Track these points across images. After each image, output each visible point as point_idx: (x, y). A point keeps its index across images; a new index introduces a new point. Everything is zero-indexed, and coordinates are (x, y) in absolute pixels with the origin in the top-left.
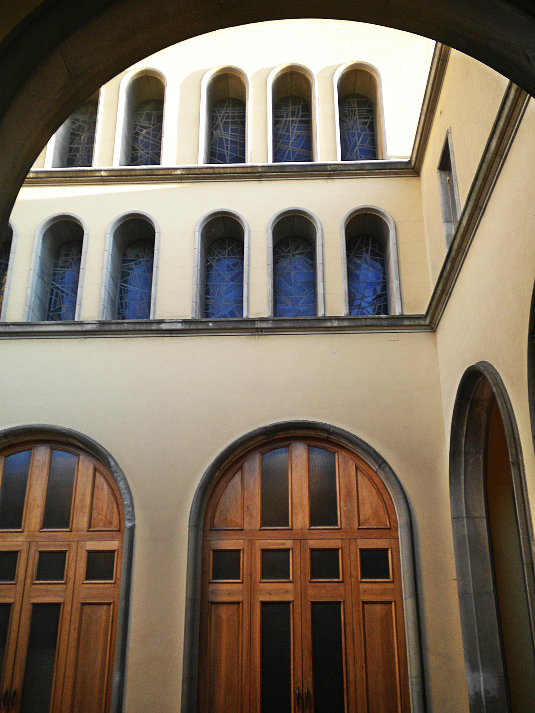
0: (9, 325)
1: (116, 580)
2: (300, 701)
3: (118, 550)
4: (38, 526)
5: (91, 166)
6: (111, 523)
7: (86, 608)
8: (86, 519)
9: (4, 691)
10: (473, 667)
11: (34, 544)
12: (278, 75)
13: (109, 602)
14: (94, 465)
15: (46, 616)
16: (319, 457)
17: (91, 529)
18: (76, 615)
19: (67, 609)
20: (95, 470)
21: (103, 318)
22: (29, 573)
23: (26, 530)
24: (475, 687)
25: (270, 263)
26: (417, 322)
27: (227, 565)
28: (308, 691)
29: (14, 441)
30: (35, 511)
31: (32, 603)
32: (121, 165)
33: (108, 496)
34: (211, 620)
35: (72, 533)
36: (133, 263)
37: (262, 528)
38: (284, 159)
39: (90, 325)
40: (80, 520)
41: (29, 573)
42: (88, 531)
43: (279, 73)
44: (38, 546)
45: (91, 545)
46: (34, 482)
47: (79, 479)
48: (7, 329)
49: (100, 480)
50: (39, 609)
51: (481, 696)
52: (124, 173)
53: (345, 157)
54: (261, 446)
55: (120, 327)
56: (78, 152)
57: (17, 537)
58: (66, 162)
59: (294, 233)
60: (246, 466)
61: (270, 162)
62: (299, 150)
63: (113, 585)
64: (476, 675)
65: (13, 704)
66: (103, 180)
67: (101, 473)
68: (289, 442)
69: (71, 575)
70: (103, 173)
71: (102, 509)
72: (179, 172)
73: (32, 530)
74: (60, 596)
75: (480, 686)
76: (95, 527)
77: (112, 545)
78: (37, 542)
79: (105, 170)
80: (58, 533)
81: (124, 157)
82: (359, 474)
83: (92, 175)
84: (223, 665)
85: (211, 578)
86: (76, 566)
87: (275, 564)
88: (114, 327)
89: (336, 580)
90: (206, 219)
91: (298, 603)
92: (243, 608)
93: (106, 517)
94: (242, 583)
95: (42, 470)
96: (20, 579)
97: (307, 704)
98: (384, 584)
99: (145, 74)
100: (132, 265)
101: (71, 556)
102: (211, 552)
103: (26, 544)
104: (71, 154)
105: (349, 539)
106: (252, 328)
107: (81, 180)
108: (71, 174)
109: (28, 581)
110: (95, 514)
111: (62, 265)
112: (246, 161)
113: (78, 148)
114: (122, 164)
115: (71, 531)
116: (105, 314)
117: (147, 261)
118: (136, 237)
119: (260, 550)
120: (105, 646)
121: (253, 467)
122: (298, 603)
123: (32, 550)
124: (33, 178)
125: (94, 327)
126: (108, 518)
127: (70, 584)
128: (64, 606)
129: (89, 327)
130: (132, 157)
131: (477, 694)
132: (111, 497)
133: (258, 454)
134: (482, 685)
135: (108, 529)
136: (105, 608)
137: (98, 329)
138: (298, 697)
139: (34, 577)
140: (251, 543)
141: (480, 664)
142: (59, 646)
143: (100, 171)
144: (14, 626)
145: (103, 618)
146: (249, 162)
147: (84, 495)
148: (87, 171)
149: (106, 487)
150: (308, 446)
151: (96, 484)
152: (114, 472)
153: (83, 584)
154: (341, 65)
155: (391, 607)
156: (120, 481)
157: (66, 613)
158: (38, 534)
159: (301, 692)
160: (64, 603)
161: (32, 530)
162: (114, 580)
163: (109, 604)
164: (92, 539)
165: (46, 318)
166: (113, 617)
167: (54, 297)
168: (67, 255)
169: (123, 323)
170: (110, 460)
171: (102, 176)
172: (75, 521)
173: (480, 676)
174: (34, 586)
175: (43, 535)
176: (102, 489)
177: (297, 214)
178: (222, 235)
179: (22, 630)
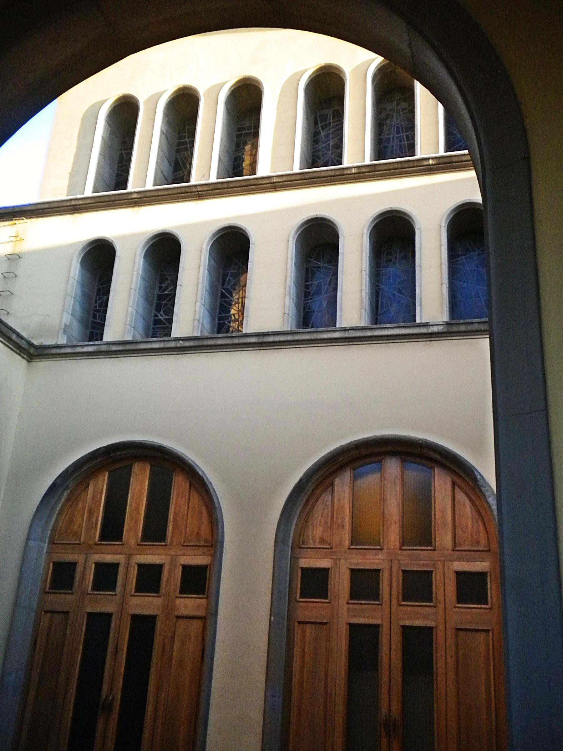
0: (348, 330)
1: (492, 604)
3: (490, 572)
4: (398, 545)
5: (414, 156)
6: (478, 543)
7: (461, 633)
8: (449, 537)
11: (395, 562)
12: (171, 98)
13: (487, 628)
14: (190, 481)
15: (143, 626)
16: (414, 474)
17: (456, 549)
18: (451, 640)
19: (385, 631)
20: (454, 484)
21: (287, 328)
22: (394, 593)
23: (385, 548)
25: (69, 292)
26: (128, 347)
27: (315, 583)
29: (364, 452)
30: (393, 527)
31: (402, 626)
32: (300, 169)
33: (472, 512)
35: (437, 551)
36: (464, 257)
37: (352, 547)
38: (321, 162)
39: (436, 327)
40: (444, 538)
41: (394, 593)
42: (454, 550)
43: (171, 95)
44: (400, 565)
45: (459, 566)
46: (388, 496)
47: (436, 494)
48: (347, 335)
49: (460, 496)
50: (136, 619)
52: (220, 186)
53: (316, 162)
54: (351, 462)
55: (470, 328)
56: (389, 142)
57: (376, 555)
58: (231, 171)
59: (393, 234)
60: (337, 482)
61: (368, 161)
62: (330, 155)
63: (328, 605)
66: (274, 186)
67: (460, 487)
68: (380, 458)
69: (440, 597)
70: (431, 162)
71: (467, 526)
72: (353, 171)
73: (392, 547)
74: (432, 620)
76: (460, 546)
77: (324, 563)
78: (399, 560)
79: (355, 167)
80: (420, 552)
81: (372, 151)
82: (457, 490)
83: (419, 164)
85: (298, 597)
86: (445, 588)
87: (365, 584)
88: (211, 342)
89: (428, 604)
90: (214, 235)
91: (441, 627)
93: (472, 535)
95: (395, 483)
96: (384, 600)
99: (244, 83)
100: (462, 259)
101: (438, 577)
102: (300, 570)
103: (387, 562)
104: (382, 146)
105: (444, 561)
106: (352, 338)
107: (407, 171)
108: (396, 166)
109: (394, 602)
110: (459, 532)
111: (384, 264)
112: (416, 154)
113: (389, 138)
114: (372, 159)
115: (434, 550)
116: (290, 324)
117: (478, 255)
118: (232, 248)
119: (348, 572)
120: (488, 676)
121: (343, 484)
122: (441, 627)
123: (394, 570)
124: (355, 173)
125: (441, 328)
126: (475, 536)
127: (441, 606)
128: (436, 629)
129: (435, 329)
130: (380, 152)
132: (475, 513)
133: (349, 470)
135: (476, 549)
136: (482, 635)
137: (445, 330)
139: (401, 598)
140: (129, 556)
143: (428, 159)
144: (384, 650)
145: (483, 647)
146: (420, 154)
147: (443, 511)
148: (123, 194)
149: (467, 502)
150: (402, 460)
151: (456, 499)
152: (481, 486)
153: (455, 607)
154: (166, 91)
156: (489, 496)
157: (439, 637)
158: (399, 552)
160: (436, 627)
161: (392, 547)
162: (490, 604)
163: (487, 631)
164: (459, 559)
165: (87, 339)
167: (380, 299)
168: (389, 254)
169: (472, 323)
170: (476, 473)
171: (429, 165)
172: (437, 539)
174: (402, 608)
175: (405, 553)
176: (464, 505)
177: (320, 222)
178: (318, 242)
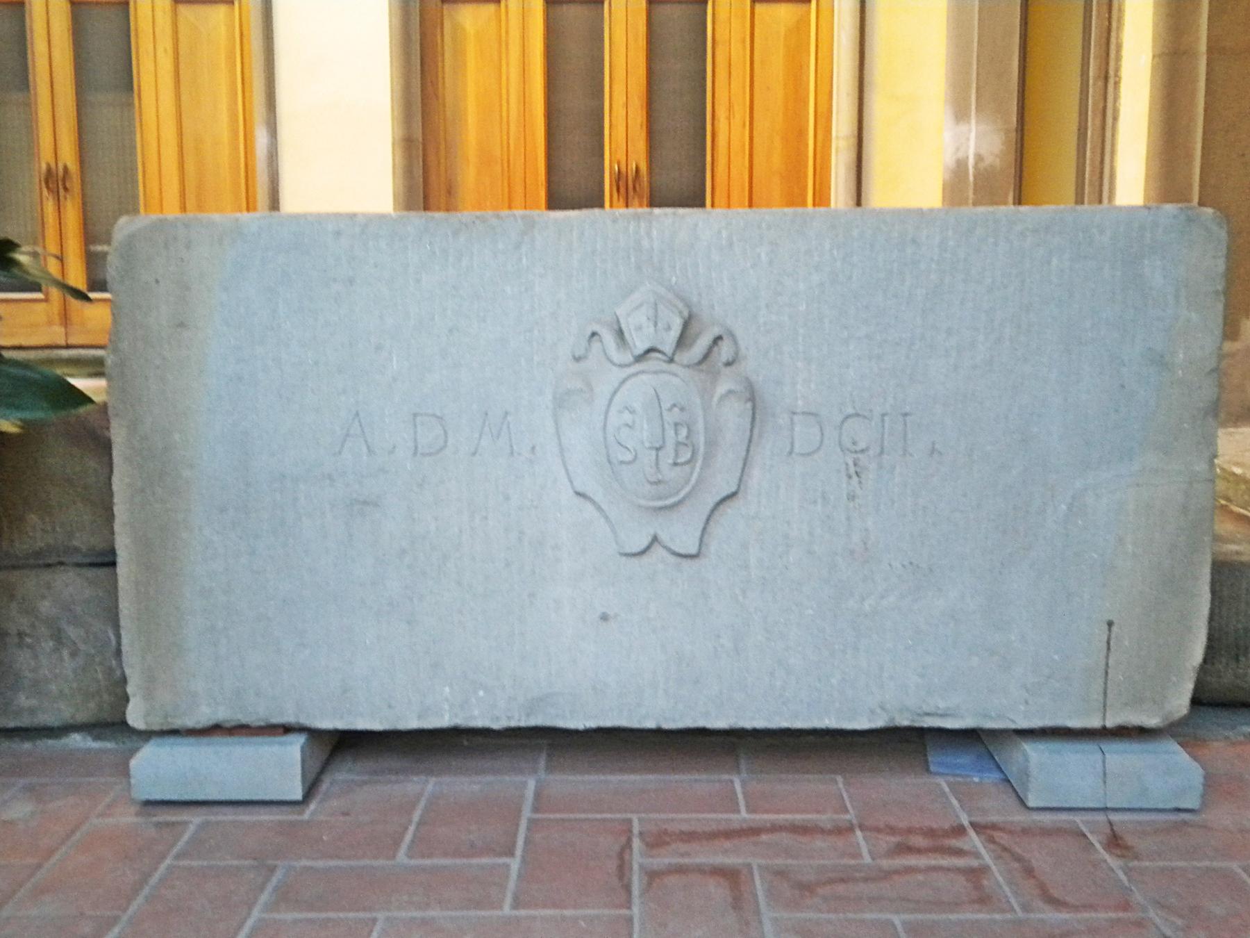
2: (622, 184)
9: (44, 166)
10: (960, 114)
24: (958, 149)
28: (637, 168)
34: (442, 35)
51: (966, 165)
64: (963, 128)
65: (66, 189)
75: (968, 146)
84: (472, 118)
92: (507, 13)
94: (46, 300)
97: (634, 188)
98: (717, 70)
131: (961, 165)
134: (972, 143)
138: (619, 178)
141: (973, 107)
142: (139, 86)
145: (223, 30)
155: (809, 12)
159: (623, 169)
166: (241, 26)
173: (970, 131)
179: (56, 54)
